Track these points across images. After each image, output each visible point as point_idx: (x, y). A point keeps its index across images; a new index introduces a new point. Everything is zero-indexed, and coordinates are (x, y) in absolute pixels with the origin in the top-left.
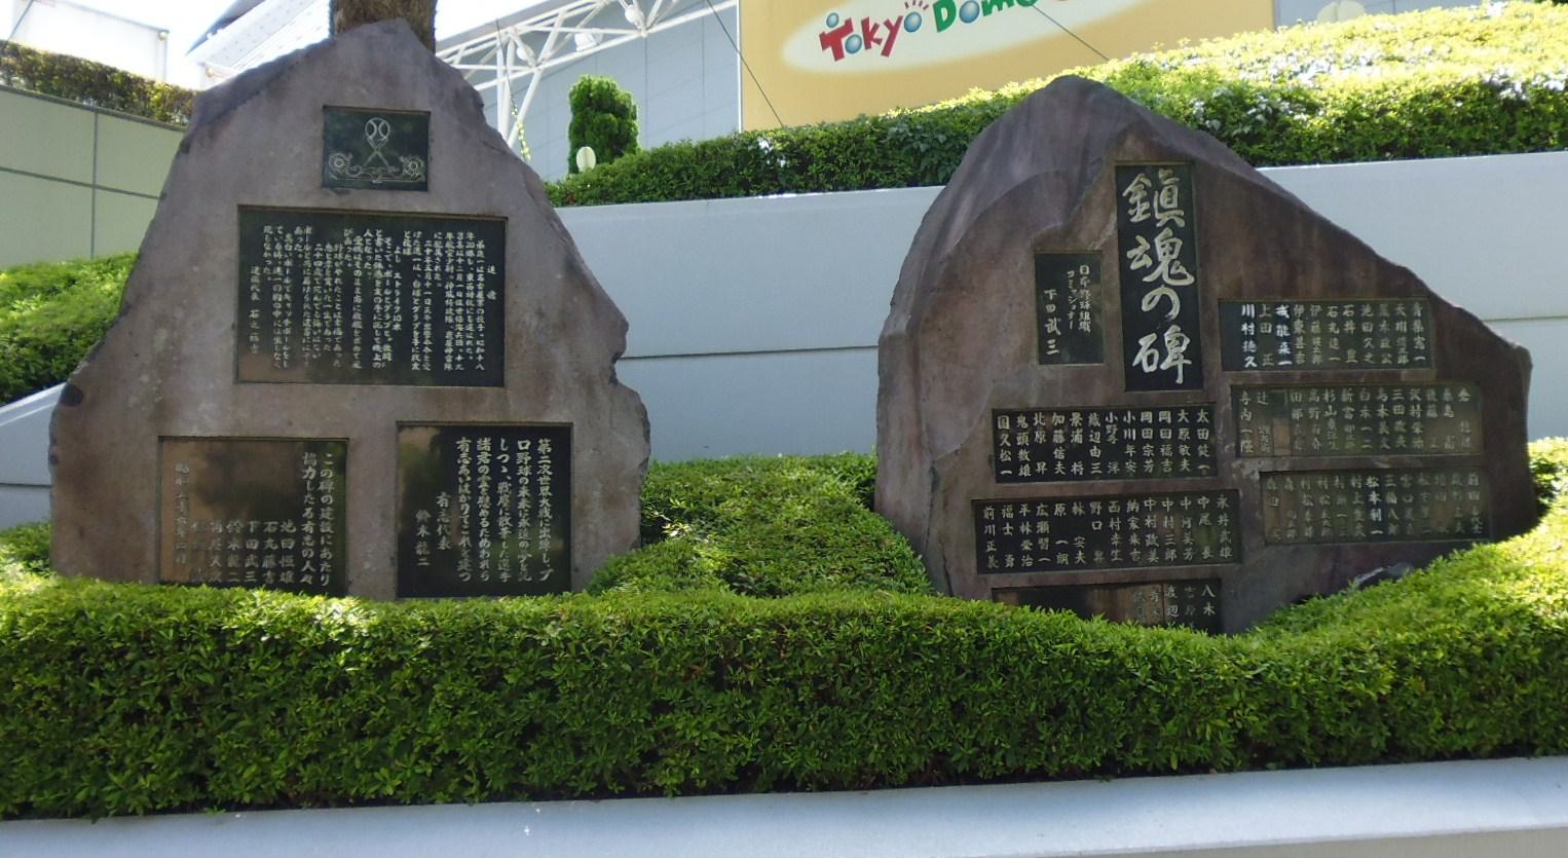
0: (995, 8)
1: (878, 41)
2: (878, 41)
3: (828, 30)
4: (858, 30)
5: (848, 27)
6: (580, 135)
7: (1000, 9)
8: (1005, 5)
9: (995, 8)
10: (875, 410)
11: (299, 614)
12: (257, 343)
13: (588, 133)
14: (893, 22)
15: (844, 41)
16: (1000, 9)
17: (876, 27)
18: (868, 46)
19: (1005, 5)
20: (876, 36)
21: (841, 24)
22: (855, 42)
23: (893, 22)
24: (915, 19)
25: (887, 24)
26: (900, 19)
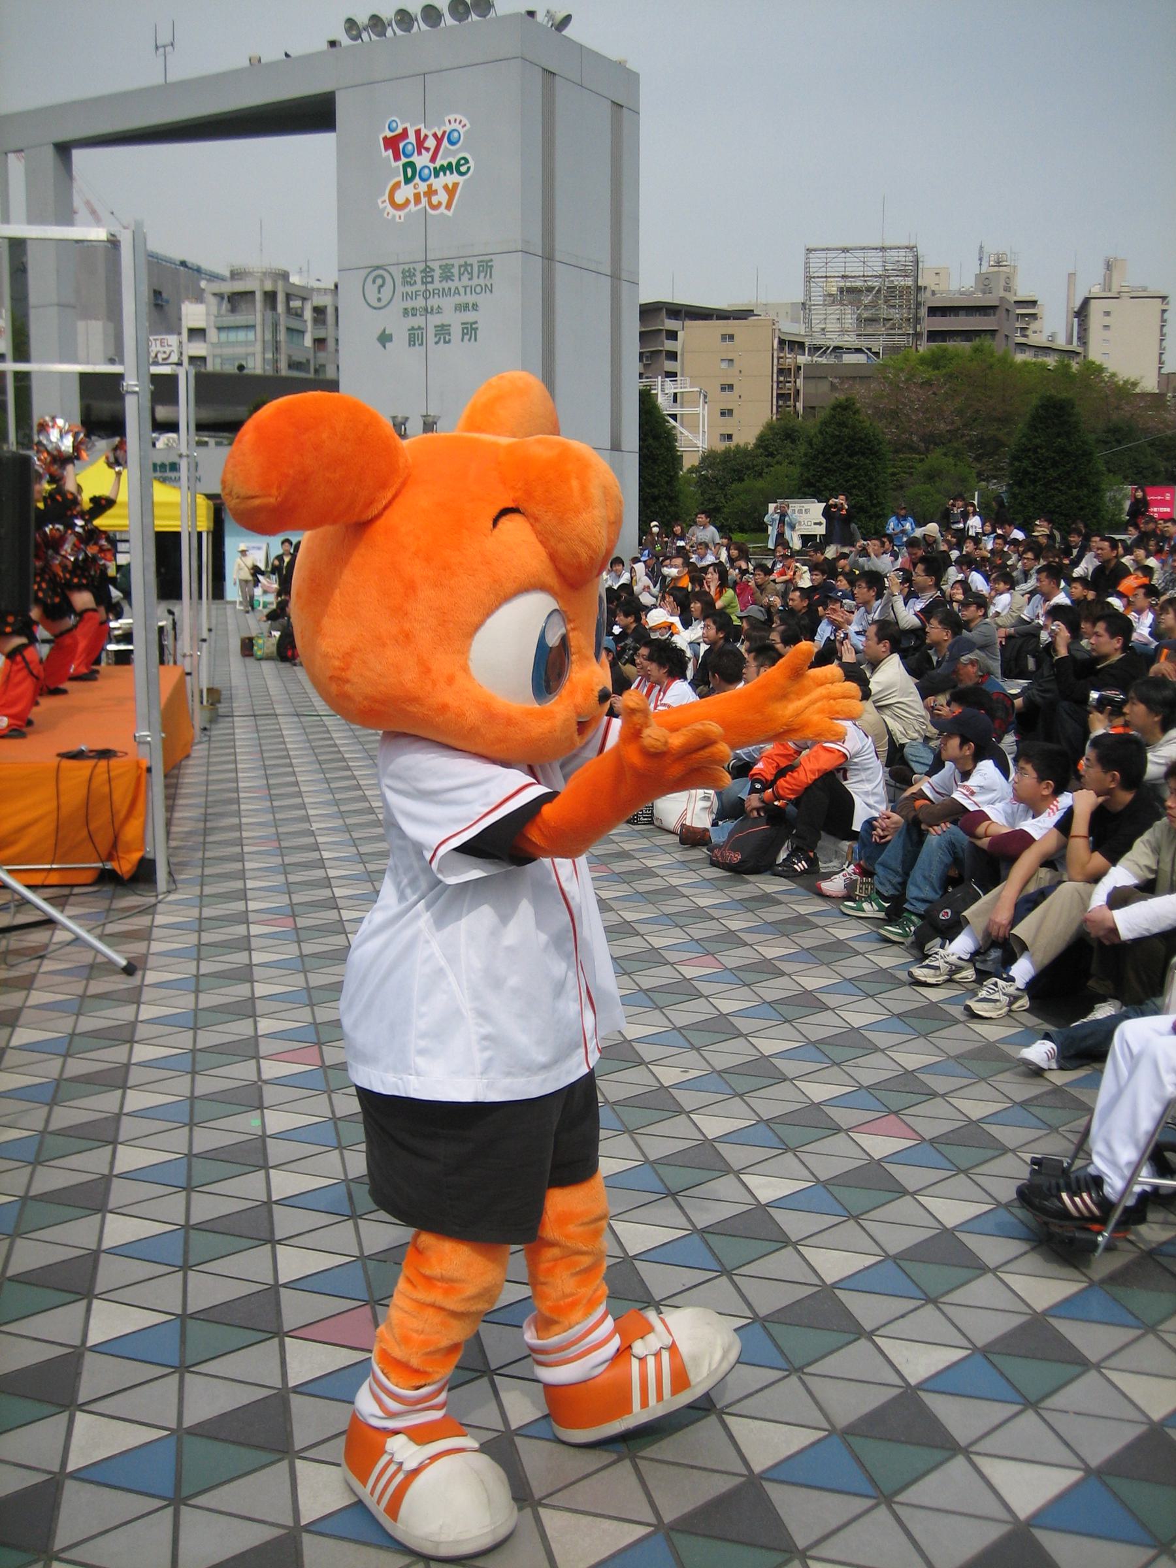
0: (442, 174)
1: (427, 149)
2: (427, 149)
3: (389, 134)
4: (412, 138)
5: (404, 134)
6: (94, 500)
7: (445, 174)
8: (448, 172)
9: (442, 174)
10: (856, 1417)
11: (497, 983)
12: (1169, 543)
13: (219, 319)
14: (439, 135)
15: (401, 145)
16: (445, 174)
17: (426, 136)
18: (420, 153)
19: (448, 172)
20: (426, 145)
21: (399, 131)
22: (410, 147)
23: (439, 135)
24: (456, 134)
25: (435, 135)
26: (444, 132)
